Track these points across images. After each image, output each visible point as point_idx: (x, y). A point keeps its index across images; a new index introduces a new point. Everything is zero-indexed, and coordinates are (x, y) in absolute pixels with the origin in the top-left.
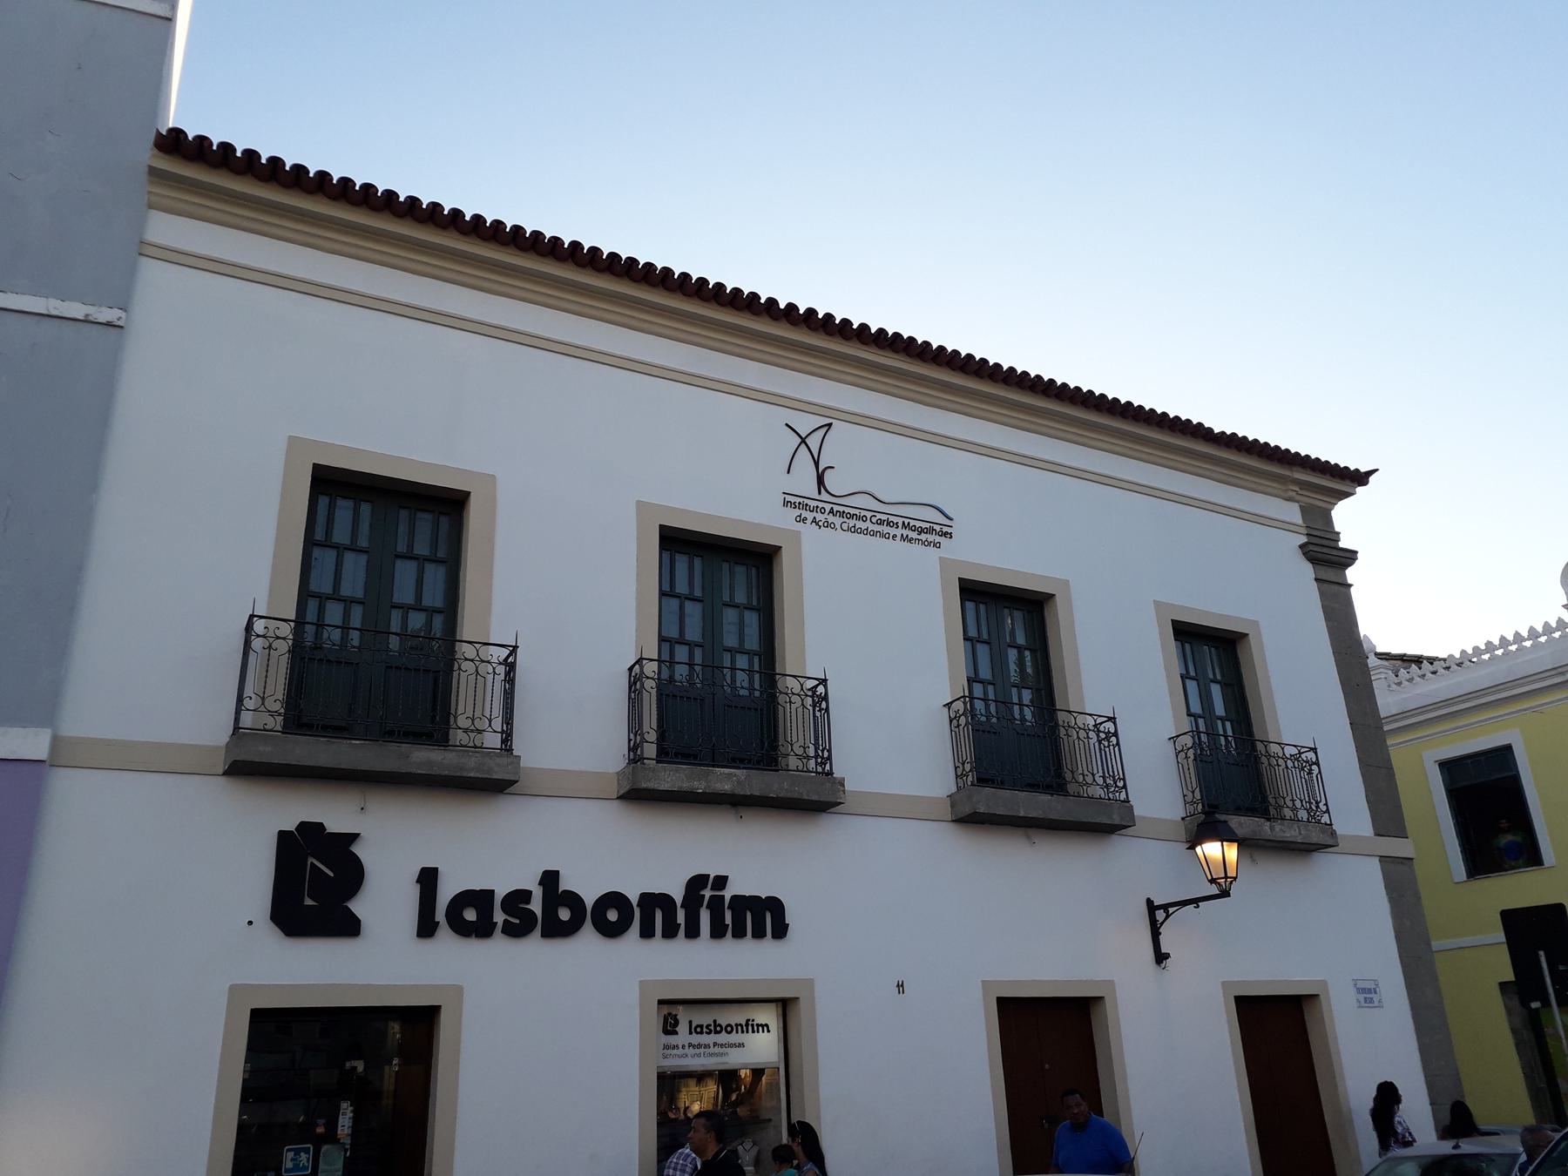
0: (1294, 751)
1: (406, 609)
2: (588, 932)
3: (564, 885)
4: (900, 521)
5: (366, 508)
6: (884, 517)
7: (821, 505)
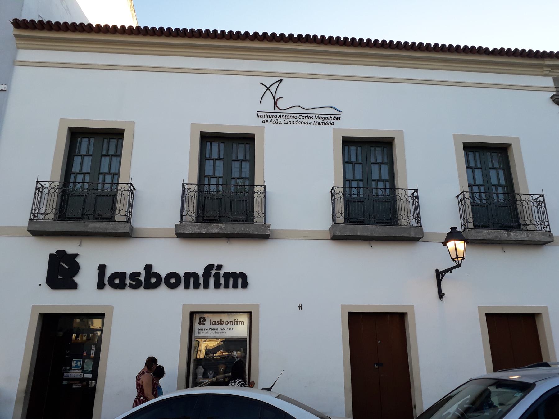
0: (535, 197)
2: (163, 287)
4: (314, 116)
5: (359, 149)
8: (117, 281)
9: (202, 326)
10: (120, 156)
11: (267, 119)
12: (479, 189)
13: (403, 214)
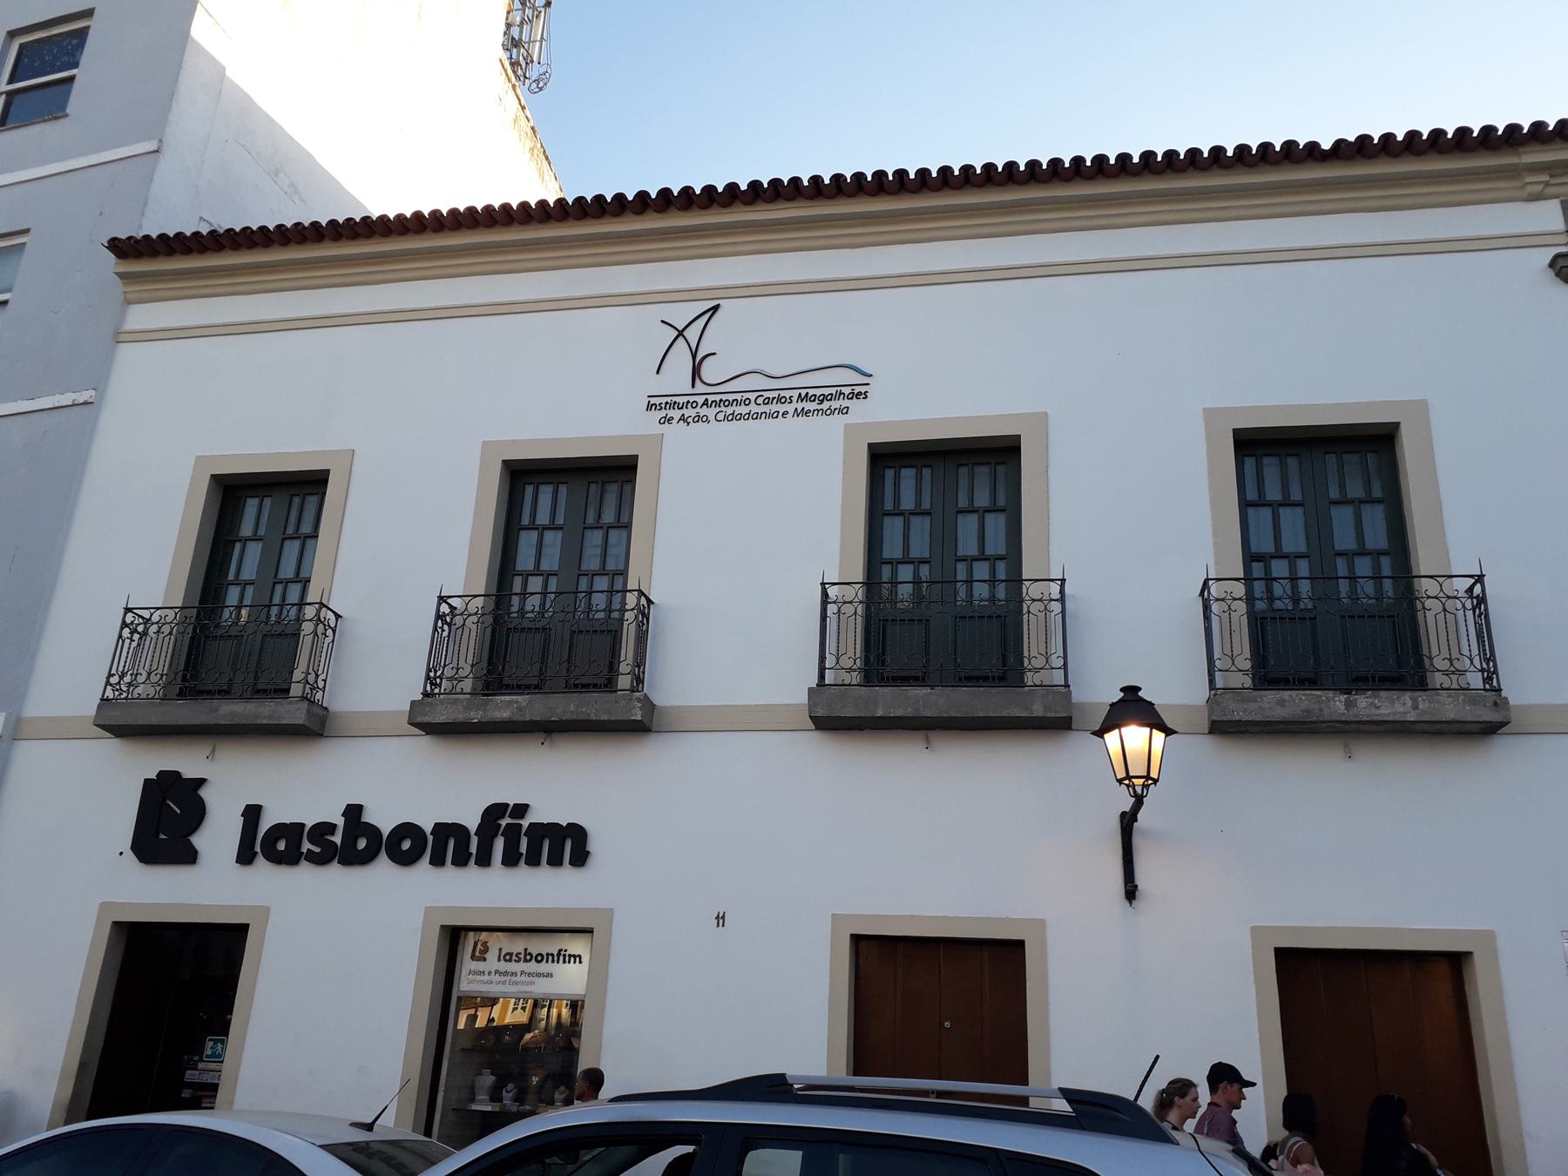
1: (527, 575)
2: (383, 860)
4: (795, 394)
5: (1292, 463)
7: (692, 399)
9: (480, 966)
10: (628, 526)
12: (1293, 568)
13: (1435, 652)
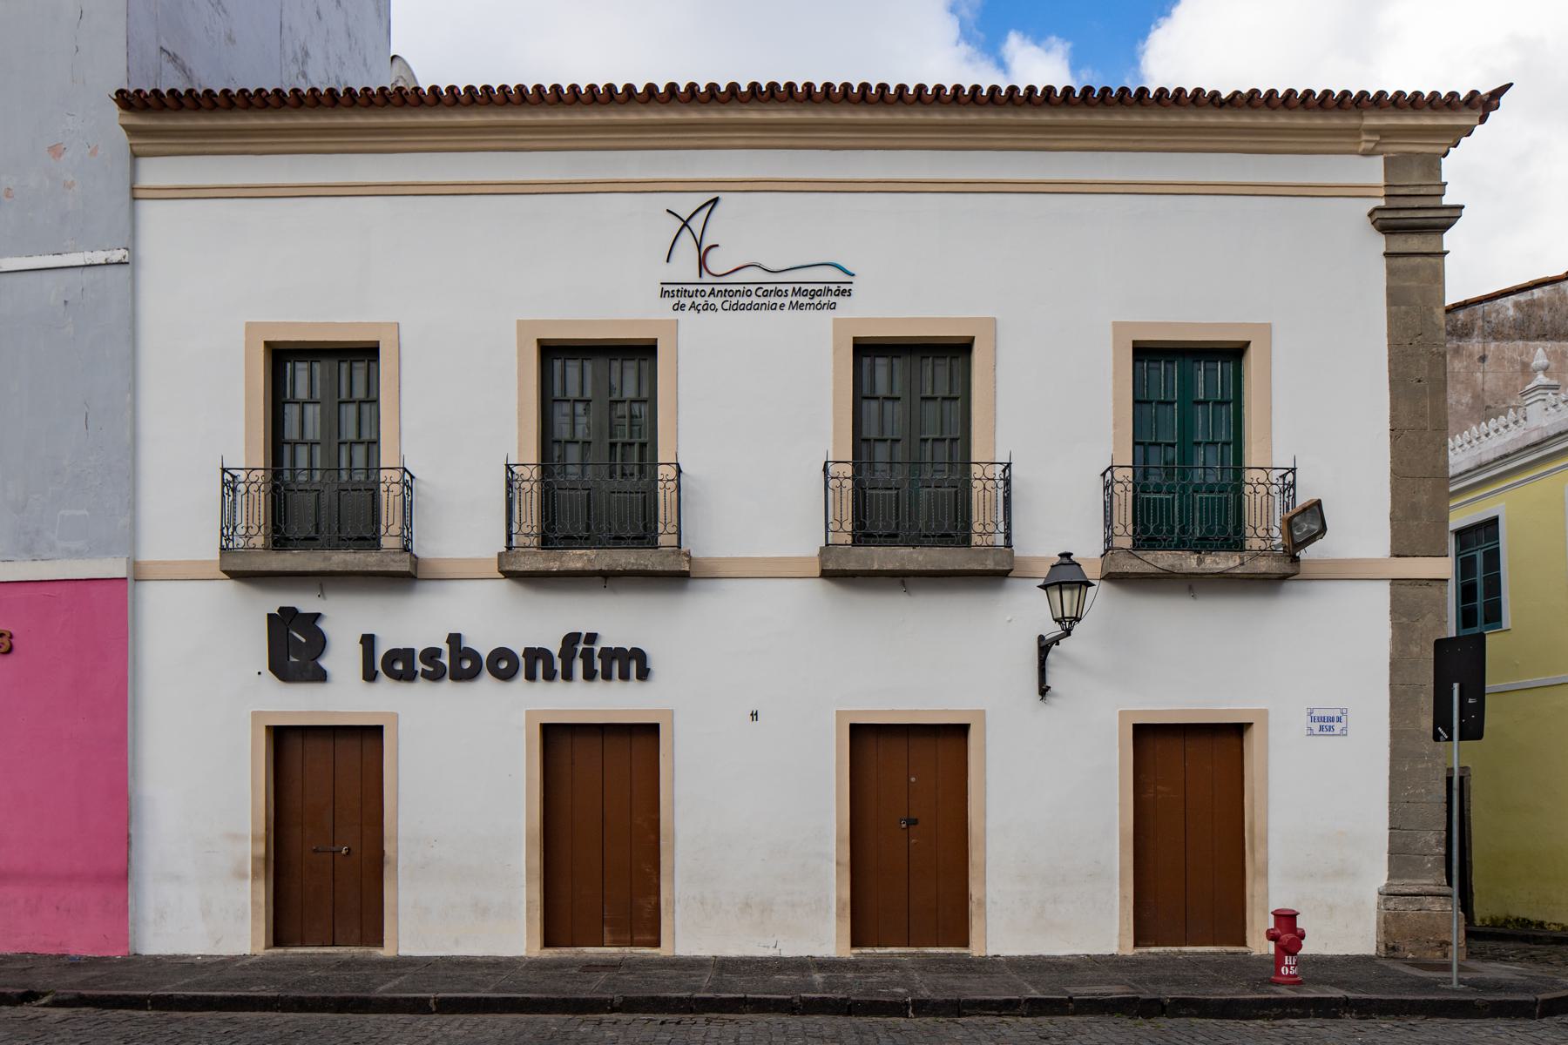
2: (486, 678)
3: (466, 644)
6: (772, 287)
7: (700, 288)
8: (399, 666)
10: (376, 401)
11: (683, 300)
